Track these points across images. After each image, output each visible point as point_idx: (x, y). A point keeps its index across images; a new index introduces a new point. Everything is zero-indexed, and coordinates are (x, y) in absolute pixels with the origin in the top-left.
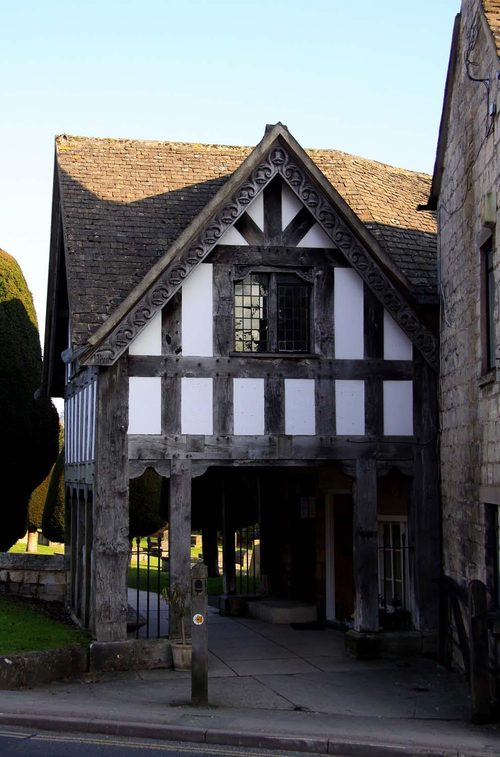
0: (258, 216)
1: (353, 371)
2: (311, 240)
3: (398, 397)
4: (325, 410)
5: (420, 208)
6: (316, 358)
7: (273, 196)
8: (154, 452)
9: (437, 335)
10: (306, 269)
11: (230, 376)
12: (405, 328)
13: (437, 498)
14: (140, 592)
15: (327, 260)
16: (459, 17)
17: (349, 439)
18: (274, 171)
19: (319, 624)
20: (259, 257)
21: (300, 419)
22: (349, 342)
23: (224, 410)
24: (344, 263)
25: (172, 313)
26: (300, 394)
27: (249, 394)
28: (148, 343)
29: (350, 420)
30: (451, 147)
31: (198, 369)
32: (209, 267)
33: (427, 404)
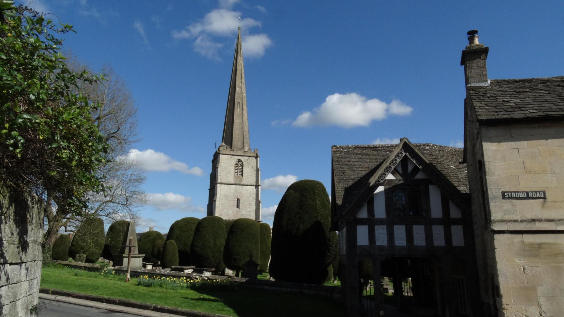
1: (438, 222)
3: (457, 232)
4: (429, 236)
5: (460, 163)
14: (377, 233)
15: (426, 183)
16: (465, 99)
18: (404, 154)
21: (419, 239)
22: (436, 211)
23: (391, 236)
24: (432, 184)
26: (419, 231)
27: (400, 231)
28: (363, 214)
29: (439, 240)
30: (468, 143)
31: (381, 222)
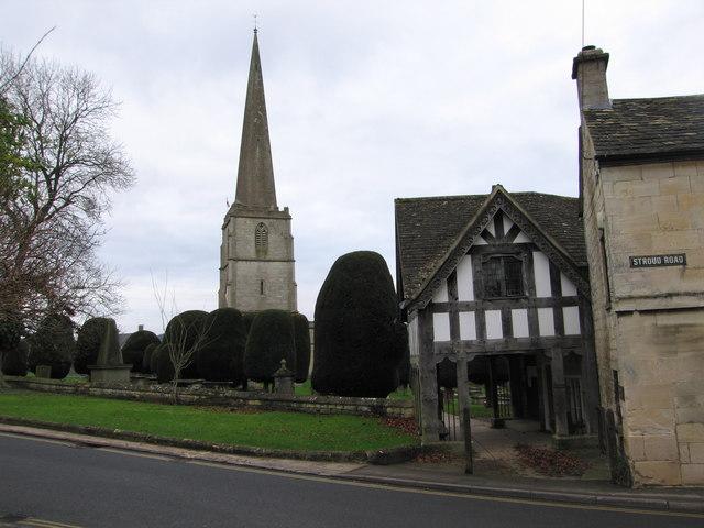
0: (492, 231)
1: (547, 303)
2: (519, 239)
3: (571, 316)
4: (533, 324)
5: (590, 64)
6: (526, 298)
7: (498, 221)
8: (446, 349)
9: (589, 282)
10: (518, 254)
11: (483, 310)
12: (571, 279)
13: (596, 364)
15: (528, 248)
17: (547, 338)
18: (498, 207)
19: (543, 430)
20: (493, 249)
21: (521, 329)
22: (543, 288)
23: (481, 327)
25: (452, 281)
26: (520, 318)
27: (493, 318)
28: (443, 297)
29: (547, 328)
31: (467, 307)
32: (469, 257)
33: (587, 318)
